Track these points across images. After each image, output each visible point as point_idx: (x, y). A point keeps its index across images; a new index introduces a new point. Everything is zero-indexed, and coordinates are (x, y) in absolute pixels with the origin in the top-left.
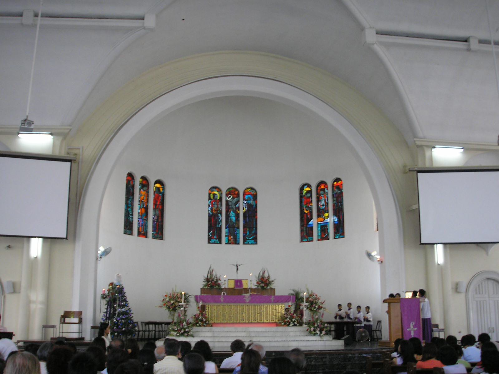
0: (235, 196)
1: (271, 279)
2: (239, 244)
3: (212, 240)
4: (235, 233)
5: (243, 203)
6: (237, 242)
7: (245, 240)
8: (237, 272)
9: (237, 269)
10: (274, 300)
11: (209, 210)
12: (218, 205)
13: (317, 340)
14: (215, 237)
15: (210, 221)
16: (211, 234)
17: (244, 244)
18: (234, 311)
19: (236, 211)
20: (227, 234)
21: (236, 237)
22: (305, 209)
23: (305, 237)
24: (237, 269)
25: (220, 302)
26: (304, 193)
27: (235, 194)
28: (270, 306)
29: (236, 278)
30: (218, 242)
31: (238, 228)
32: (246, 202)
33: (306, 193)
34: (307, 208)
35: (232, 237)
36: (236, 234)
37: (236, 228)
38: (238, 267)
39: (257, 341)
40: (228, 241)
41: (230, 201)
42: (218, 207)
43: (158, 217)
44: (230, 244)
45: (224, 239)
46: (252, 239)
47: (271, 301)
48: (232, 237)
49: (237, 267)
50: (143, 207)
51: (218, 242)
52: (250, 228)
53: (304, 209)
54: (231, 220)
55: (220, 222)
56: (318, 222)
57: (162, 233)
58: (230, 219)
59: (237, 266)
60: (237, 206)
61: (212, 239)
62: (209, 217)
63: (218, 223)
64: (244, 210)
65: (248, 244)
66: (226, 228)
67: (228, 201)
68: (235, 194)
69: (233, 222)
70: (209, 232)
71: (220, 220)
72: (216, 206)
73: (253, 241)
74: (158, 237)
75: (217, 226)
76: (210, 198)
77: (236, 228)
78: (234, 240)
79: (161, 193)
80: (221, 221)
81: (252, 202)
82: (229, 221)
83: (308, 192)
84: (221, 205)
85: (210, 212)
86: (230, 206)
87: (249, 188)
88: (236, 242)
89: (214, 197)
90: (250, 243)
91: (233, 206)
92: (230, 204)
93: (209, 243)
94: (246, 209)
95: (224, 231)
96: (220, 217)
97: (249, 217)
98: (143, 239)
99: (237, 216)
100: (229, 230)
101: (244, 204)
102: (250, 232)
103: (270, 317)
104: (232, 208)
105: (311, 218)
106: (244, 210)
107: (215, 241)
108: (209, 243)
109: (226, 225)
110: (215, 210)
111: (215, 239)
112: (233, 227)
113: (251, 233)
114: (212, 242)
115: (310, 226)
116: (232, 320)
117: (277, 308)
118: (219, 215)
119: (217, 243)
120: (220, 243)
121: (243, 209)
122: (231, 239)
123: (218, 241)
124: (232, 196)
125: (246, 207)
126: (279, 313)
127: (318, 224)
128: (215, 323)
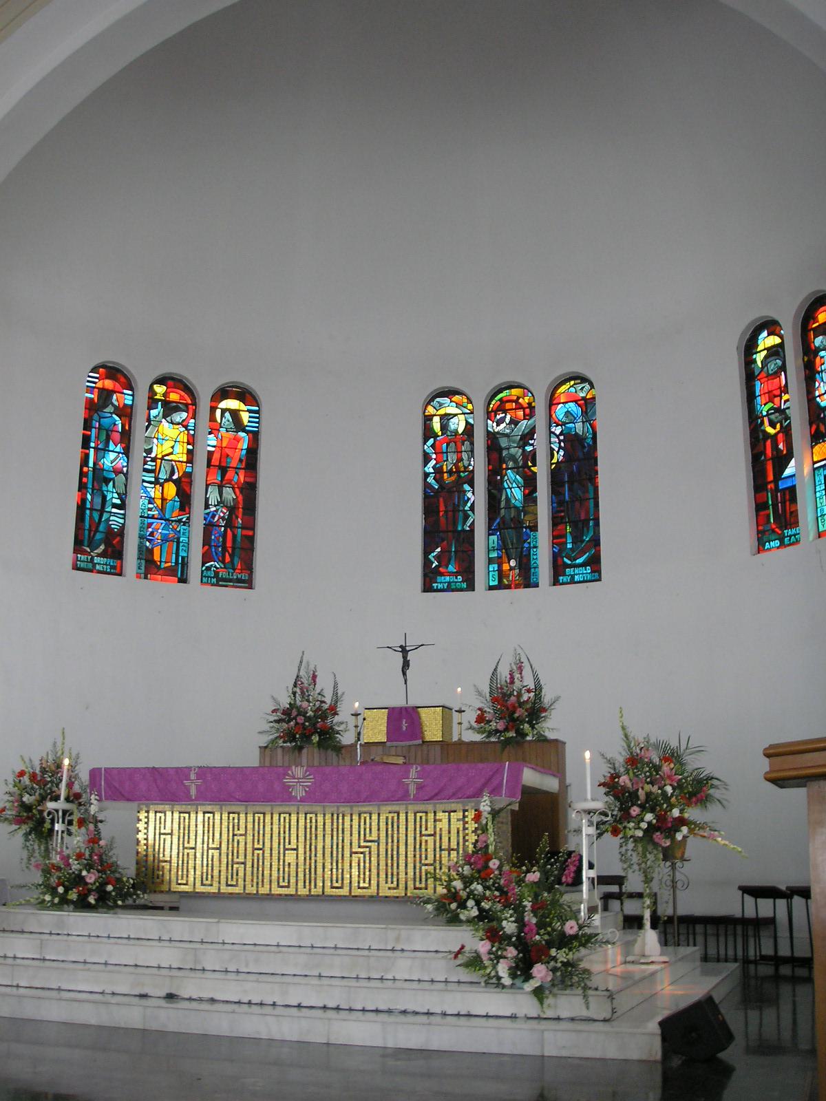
0: (520, 413)
1: (547, 697)
2: (536, 585)
3: (440, 579)
4: (526, 545)
5: (551, 432)
6: (533, 579)
7: (558, 571)
8: (404, 674)
9: (406, 664)
10: (420, 788)
11: (426, 475)
12: (459, 452)
13: (521, 1014)
14: (451, 568)
15: (430, 509)
16: (438, 558)
17: (556, 582)
18: (250, 838)
19: (525, 465)
20: (494, 555)
21: (529, 560)
22: (766, 420)
23: (773, 531)
24: (406, 664)
25: (404, 797)
26: (759, 358)
27: (520, 407)
28: (200, 816)
29: (399, 702)
30: (464, 585)
31: (534, 528)
32: (558, 430)
33: (766, 357)
34: (772, 417)
35: (513, 563)
36: (529, 549)
37: (526, 528)
38: (410, 656)
39: (200, 1000)
40: (500, 580)
41: (507, 435)
42: (460, 460)
43: (232, 510)
44: (508, 587)
45: (483, 572)
46: (583, 565)
47: (407, 791)
48: (513, 563)
49: (405, 657)
50: (169, 479)
51: (464, 585)
52: (574, 524)
53: (762, 422)
54: (508, 500)
55: (470, 513)
56: (815, 463)
57: (249, 566)
58: (504, 497)
59: (404, 650)
60: (529, 448)
61: (442, 574)
62: (426, 497)
63: (461, 514)
64: (555, 461)
65: (572, 582)
66: (491, 532)
67: (498, 433)
68: (520, 407)
69: (516, 507)
70: (427, 551)
71: (469, 505)
72: (452, 458)
73: (589, 569)
74: (230, 581)
75: (460, 528)
76: (428, 433)
77: (526, 528)
78: (519, 575)
79: (244, 431)
80: (472, 508)
81: (579, 427)
82: (503, 504)
83: (774, 352)
84: (472, 452)
85: (430, 480)
86: (504, 453)
87: (569, 380)
88: (527, 579)
89: (444, 427)
90: (577, 578)
91: (513, 451)
92: (503, 442)
93: (427, 588)
94: (559, 456)
95: (483, 543)
96: (469, 495)
97: (571, 483)
98: (170, 587)
99: (530, 483)
100: (502, 539)
101: (554, 439)
102: (577, 539)
103: (406, 872)
104: (513, 458)
105: (789, 456)
106: (555, 461)
107: (449, 583)
108: (427, 588)
109: (491, 520)
110: (450, 472)
111: (451, 574)
112: (517, 524)
113: (583, 541)
114: (440, 586)
115: (788, 484)
116: (241, 882)
117: (443, 825)
118: (466, 487)
119: (461, 590)
120: (471, 587)
121: (552, 457)
122: (511, 569)
123: (463, 581)
124: (508, 417)
125: (560, 448)
126: (450, 850)
127: (815, 469)
128: (195, 895)
